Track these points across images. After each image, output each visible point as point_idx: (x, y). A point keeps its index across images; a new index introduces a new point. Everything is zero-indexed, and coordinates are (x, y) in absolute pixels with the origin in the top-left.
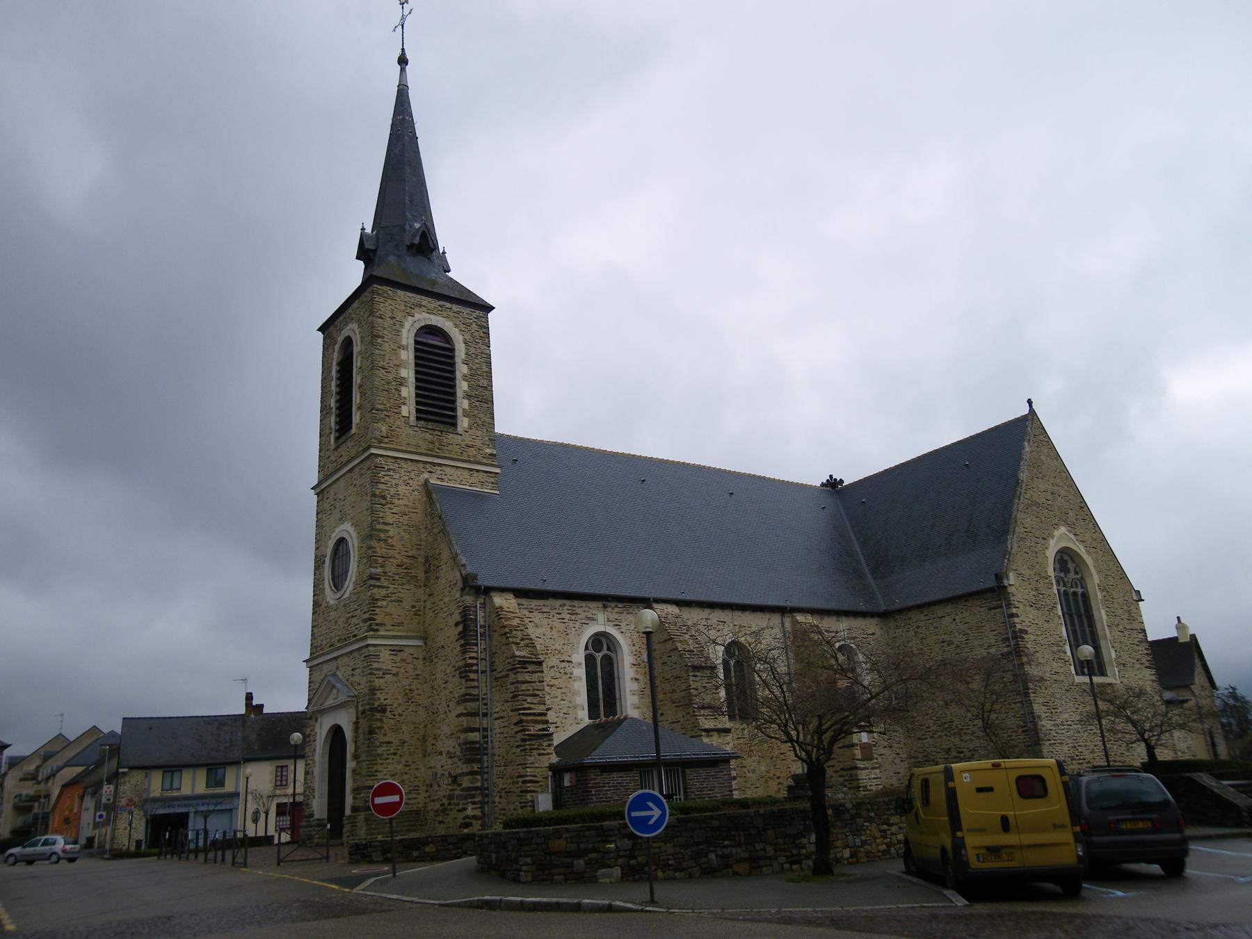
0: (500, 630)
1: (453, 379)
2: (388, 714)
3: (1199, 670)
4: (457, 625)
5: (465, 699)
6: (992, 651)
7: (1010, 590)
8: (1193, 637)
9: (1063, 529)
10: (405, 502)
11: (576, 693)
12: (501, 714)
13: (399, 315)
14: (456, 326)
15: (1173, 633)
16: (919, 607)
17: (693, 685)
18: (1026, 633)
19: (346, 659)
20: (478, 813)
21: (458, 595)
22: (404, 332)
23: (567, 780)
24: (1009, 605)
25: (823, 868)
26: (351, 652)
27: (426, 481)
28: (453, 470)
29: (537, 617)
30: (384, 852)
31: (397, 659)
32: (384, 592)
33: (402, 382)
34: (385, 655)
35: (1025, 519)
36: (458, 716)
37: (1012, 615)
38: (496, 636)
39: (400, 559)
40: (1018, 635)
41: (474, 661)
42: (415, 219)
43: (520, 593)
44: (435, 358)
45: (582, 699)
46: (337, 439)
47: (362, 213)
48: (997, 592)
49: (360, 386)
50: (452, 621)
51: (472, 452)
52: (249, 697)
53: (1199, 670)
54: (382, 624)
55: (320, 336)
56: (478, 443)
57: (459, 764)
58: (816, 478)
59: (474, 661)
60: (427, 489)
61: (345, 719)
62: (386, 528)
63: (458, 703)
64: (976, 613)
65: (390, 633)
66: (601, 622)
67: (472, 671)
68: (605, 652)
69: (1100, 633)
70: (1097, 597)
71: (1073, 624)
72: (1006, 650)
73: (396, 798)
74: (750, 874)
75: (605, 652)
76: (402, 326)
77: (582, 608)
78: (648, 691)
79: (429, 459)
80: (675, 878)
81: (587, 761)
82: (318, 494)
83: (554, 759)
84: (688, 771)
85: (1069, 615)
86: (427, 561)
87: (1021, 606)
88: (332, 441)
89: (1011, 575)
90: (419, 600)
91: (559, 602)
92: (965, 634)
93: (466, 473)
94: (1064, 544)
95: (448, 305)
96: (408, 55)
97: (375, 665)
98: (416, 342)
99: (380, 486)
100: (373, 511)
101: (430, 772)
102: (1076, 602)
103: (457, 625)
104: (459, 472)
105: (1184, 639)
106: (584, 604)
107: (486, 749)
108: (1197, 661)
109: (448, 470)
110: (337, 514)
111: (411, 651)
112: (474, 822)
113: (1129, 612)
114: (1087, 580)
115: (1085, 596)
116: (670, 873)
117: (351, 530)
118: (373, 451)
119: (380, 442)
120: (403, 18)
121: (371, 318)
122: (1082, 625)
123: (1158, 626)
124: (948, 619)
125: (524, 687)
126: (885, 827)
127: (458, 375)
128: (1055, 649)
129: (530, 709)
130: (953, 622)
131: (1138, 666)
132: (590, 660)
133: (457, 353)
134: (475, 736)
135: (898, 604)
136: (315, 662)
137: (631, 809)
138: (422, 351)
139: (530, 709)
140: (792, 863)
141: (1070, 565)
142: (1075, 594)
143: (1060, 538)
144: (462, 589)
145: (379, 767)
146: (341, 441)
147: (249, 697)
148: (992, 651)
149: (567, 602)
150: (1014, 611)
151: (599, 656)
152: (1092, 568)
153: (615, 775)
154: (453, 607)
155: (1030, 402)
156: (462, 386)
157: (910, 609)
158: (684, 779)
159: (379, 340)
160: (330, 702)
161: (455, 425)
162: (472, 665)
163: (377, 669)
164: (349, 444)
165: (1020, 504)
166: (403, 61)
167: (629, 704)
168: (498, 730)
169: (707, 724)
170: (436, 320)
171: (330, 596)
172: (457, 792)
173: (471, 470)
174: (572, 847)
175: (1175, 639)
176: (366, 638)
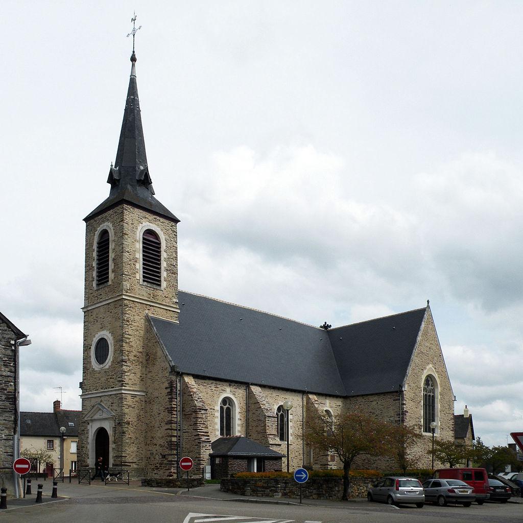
1: (160, 260)
3: (469, 430)
6: (392, 419)
8: (471, 415)
9: (431, 366)
11: (216, 424)
12: (188, 431)
16: (362, 396)
18: (407, 412)
20: (175, 471)
23: (217, 461)
27: (147, 315)
28: (159, 309)
29: (201, 387)
33: (136, 260)
34: (129, 397)
35: (415, 359)
37: (404, 404)
38: (186, 395)
39: (135, 353)
40: (404, 413)
41: (175, 406)
43: (196, 377)
45: (218, 426)
47: (108, 156)
51: (168, 300)
53: (469, 430)
56: (170, 296)
58: (318, 324)
59: (175, 406)
60: (148, 319)
61: (108, 426)
62: (129, 337)
64: (388, 401)
65: (131, 389)
66: (228, 392)
67: (174, 411)
68: (227, 406)
70: (438, 397)
71: (426, 410)
72: (398, 419)
73: (190, 464)
74: (317, 499)
75: (227, 406)
76: (137, 229)
77: (221, 386)
80: (296, 498)
81: (229, 454)
82: (85, 312)
83: (211, 452)
87: (408, 400)
88: (94, 285)
89: (406, 386)
92: (379, 410)
95: (158, 218)
96: (136, 56)
99: (127, 316)
102: (429, 399)
103: (166, 388)
104: (162, 310)
105: (466, 416)
106: (221, 383)
107: (179, 445)
109: (156, 309)
110: (98, 325)
111: (140, 397)
112: (174, 475)
114: (436, 390)
115: (433, 397)
119: (127, 292)
120: (134, 30)
121: (121, 223)
122: (429, 410)
123: (459, 409)
125: (200, 420)
126: (359, 487)
128: (417, 420)
129: (202, 430)
132: (221, 408)
137: (295, 475)
138: (145, 242)
139: (202, 430)
140: (329, 496)
141: (430, 383)
142: (430, 395)
143: (429, 370)
144: (171, 372)
145: (127, 448)
148: (392, 419)
149: (214, 382)
151: (225, 407)
152: (439, 384)
153: (238, 461)
155: (428, 302)
156: (164, 264)
157: (358, 396)
161: (160, 285)
163: (126, 405)
166: (133, 59)
167: (236, 430)
168: (185, 437)
170: (153, 227)
172: (165, 462)
173: (167, 310)
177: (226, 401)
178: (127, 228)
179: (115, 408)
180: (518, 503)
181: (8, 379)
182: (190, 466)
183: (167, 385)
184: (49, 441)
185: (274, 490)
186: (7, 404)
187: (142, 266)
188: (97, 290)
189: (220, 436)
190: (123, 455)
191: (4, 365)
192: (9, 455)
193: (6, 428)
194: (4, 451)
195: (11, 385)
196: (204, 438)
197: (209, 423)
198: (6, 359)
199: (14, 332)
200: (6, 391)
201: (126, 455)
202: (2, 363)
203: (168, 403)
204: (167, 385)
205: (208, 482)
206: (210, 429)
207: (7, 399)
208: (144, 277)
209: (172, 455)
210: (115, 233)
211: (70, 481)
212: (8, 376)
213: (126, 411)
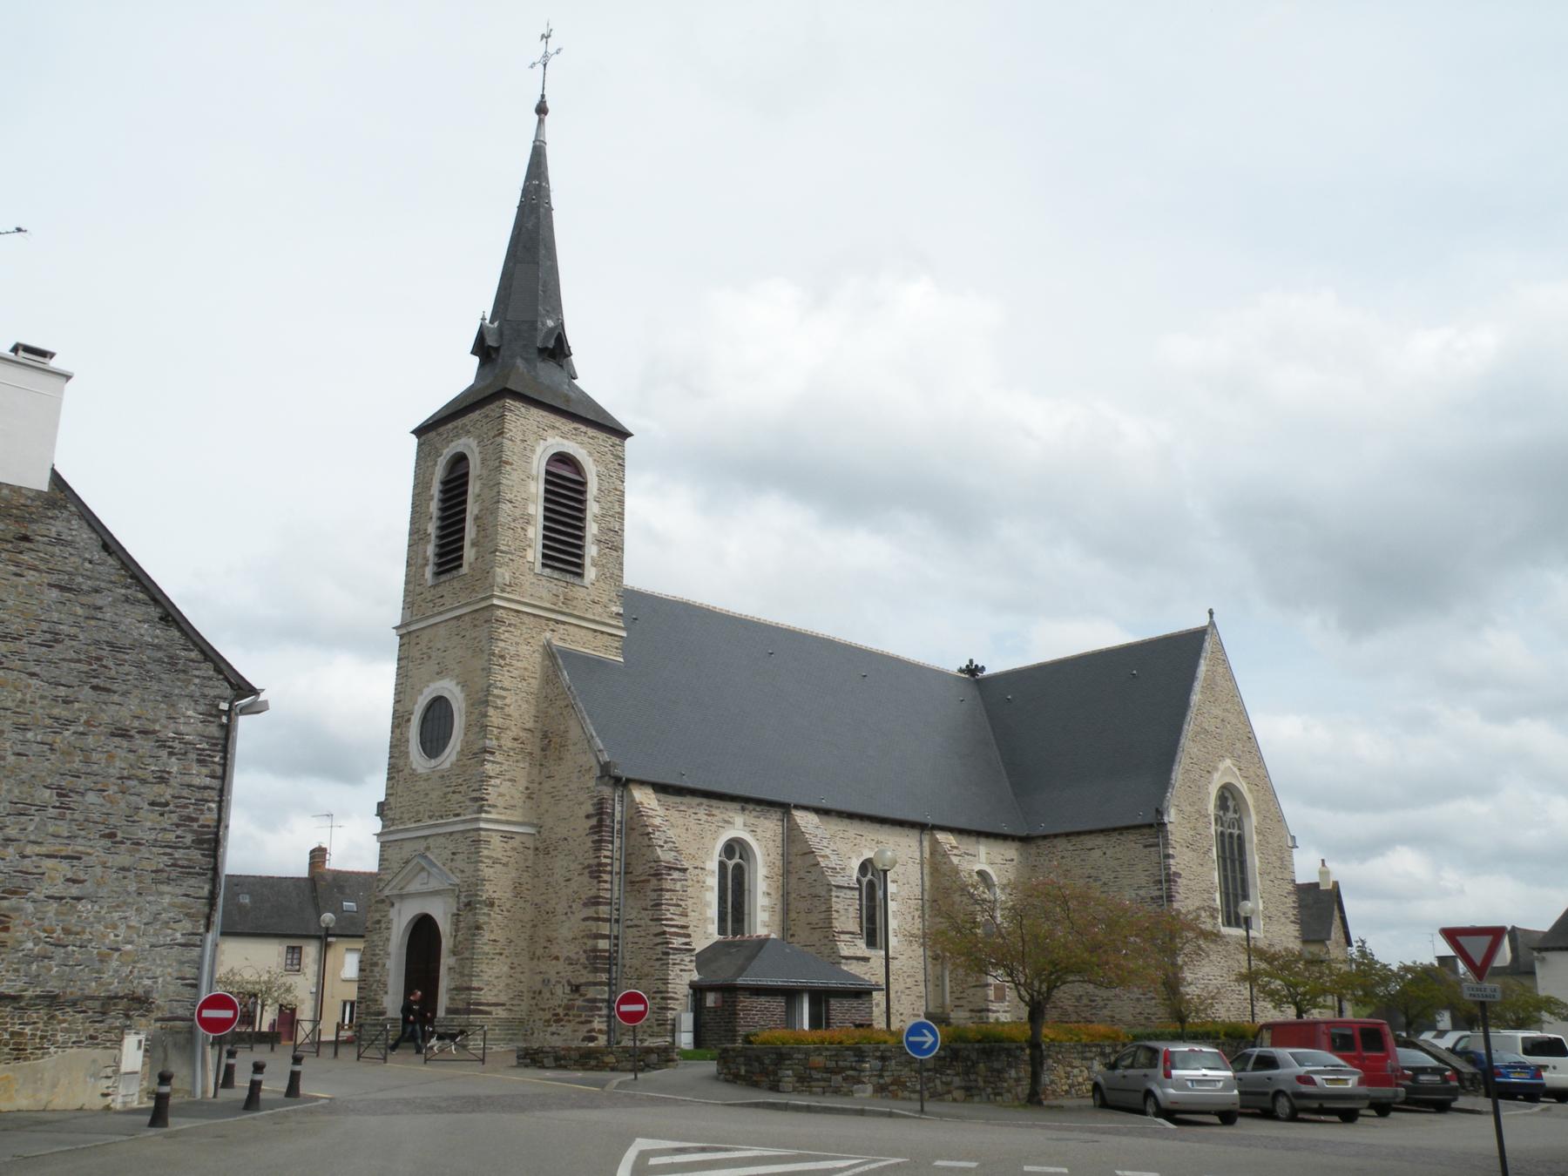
0: (636, 825)
2: (496, 909)
3: (1337, 922)
4: (588, 817)
6: (1142, 893)
7: (1169, 827)
8: (1336, 884)
9: (1228, 762)
11: (708, 905)
12: (635, 922)
14: (590, 454)
15: (1315, 879)
16: (1067, 835)
18: (1179, 875)
19: (442, 840)
21: (592, 783)
22: (535, 458)
23: (710, 1000)
24: (1166, 844)
25: (1034, 1099)
26: (451, 834)
30: (557, 1059)
32: (497, 768)
34: (496, 840)
35: (1190, 747)
36: (585, 919)
39: (515, 732)
42: (548, 314)
43: (661, 789)
44: (565, 488)
46: (437, 574)
48: (1157, 827)
49: (477, 518)
50: (582, 813)
51: (599, 609)
53: (1337, 922)
54: (494, 806)
55: (414, 440)
56: (605, 599)
57: (584, 972)
58: (953, 663)
60: (550, 653)
62: (503, 693)
63: (585, 905)
64: (1131, 847)
65: (503, 818)
66: (738, 825)
68: (737, 860)
69: (1250, 881)
71: (1225, 870)
72: (1157, 893)
73: (640, 1008)
74: (964, 1101)
75: (737, 860)
76: (533, 451)
77: (723, 811)
79: (554, 616)
81: (740, 981)
82: (401, 637)
83: (695, 976)
84: (832, 1001)
85: (1222, 858)
89: (1173, 811)
90: (532, 782)
91: (698, 800)
93: (590, 634)
94: (1227, 779)
95: (583, 428)
97: (486, 852)
98: (548, 472)
99: (501, 644)
101: (539, 978)
102: (1231, 844)
103: (588, 817)
108: (1336, 913)
109: (571, 629)
113: (1281, 859)
114: (1245, 821)
115: (1240, 838)
116: (906, 1094)
117: (457, 690)
120: (546, 56)
122: (1234, 871)
123: (1305, 868)
124: (1097, 853)
127: (589, 516)
128: (1206, 896)
130: (1102, 856)
131: (1283, 920)
134: (603, 944)
135: (1043, 828)
136: (392, 838)
138: (551, 479)
141: (1231, 803)
142: (1231, 835)
143: (1225, 772)
146: (443, 578)
148: (1142, 893)
149: (705, 801)
150: (1171, 851)
151: (731, 864)
154: (583, 797)
155: (1211, 613)
156: (592, 529)
158: (828, 1010)
159: (508, 468)
160: (414, 887)
161: (581, 575)
162: (606, 865)
164: (455, 583)
165: (1189, 729)
166: (542, 110)
169: (845, 951)
171: (417, 759)
172: (579, 1003)
174: (833, 1064)
175: (1317, 885)
176: (478, 820)
177: (731, 848)
178: (511, 449)
182: (640, 1015)
183: (591, 810)
186: (196, 855)
187: (541, 532)
188: (434, 586)
189: (716, 937)
190: (475, 984)
191: (199, 761)
194: (175, 974)
195: (210, 809)
197: (690, 902)
199: (230, 683)
200: (195, 825)
204: (591, 810)
205: (686, 1055)
207: (198, 842)
208: (545, 556)
209: (595, 984)
210: (483, 461)
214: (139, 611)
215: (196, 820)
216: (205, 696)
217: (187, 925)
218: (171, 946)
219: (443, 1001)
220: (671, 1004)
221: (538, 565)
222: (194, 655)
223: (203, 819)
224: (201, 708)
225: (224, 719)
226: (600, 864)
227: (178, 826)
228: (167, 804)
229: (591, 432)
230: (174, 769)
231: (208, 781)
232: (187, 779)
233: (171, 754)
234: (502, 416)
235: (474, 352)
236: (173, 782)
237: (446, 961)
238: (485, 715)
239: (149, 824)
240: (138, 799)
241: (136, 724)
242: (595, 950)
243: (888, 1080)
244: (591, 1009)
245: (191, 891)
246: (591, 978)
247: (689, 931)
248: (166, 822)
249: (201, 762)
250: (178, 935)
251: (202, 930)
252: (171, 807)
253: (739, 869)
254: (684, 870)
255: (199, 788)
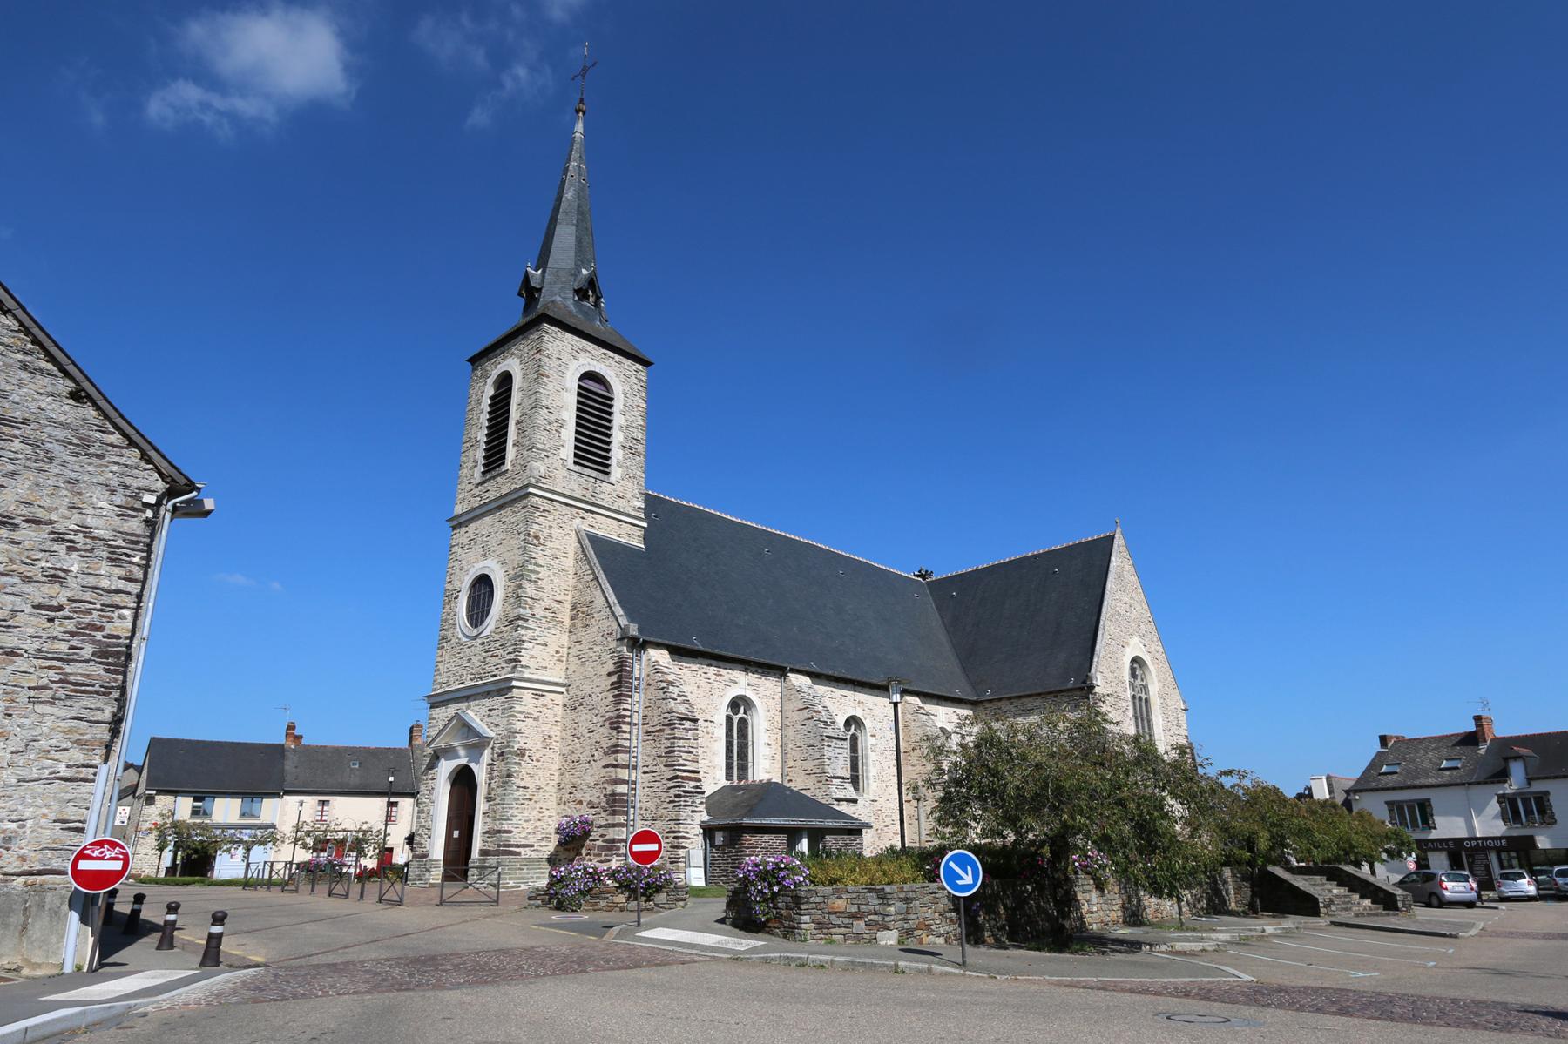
4: (609, 674)
5: (615, 749)
10: (556, 545)
13: (565, 358)
17: (827, 755)
22: (569, 374)
23: (719, 838)
31: (538, 703)
32: (530, 633)
46: (484, 473)
48: (1087, 688)
52: (291, 727)
56: (628, 496)
63: (606, 753)
73: (654, 847)
78: (779, 757)
83: (705, 817)
84: (828, 838)
86: (574, 607)
97: (518, 708)
98: (580, 387)
100: (524, 551)
103: (609, 674)
115: (1147, 700)
118: (531, 490)
125: (680, 743)
132: (729, 720)
133: (615, 403)
134: (622, 789)
138: (582, 392)
145: (516, 812)
147: (291, 727)
151: (736, 719)
153: (766, 837)
154: (606, 657)
174: (854, 909)
177: (736, 703)
178: (549, 365)
179: (497, 720)
180: (1444, 935)
181: (118, 599)
182: (652, 856)
183: (612, 668)
184: (392, 804)
185: (876, 923)
186: (97, 670)
187: (573, 435)
188: (481, 483)
189: (724, 782)
190: (505, 827)
191: (111, 560)
192: (69, 829)
193: (77, 742)
194: (53, 816)
195: (121, 617)
196: (690, 785)
197: (700, 751)
198: (120, 542)
199: (160, 474)
200: (99, 636)
201: (510, 828)
202: (105, 554)
203: (612, 707)
204: (612, 668)
205: (697, 892)
206: (702, 766)
207: (102, 654)
208: (576, 455)
209: (614, 826)
210: (525, 375)
211: (362, 895)
212: (118, 592)
213: (518, 725)
214: (42, 382)
215: (101, 629)
216: (125, 486)
217: (78, 756)
218: (49, 780)
219: (477, 844)
220: (684, 843)
221: (571, 459)
222: (115, 438)
223: (110, 629)
224: (119, 499)
225: (149, 514)
226: (619, 716)
227: (73, 634)
228: (60, 608)
229: (618, 358)
230: (75, 568)
231: (121, 585)
232: (91, 581)
233: (70, 549)
234: (541, 337)
235: (520, 294)
236: (70, 582)
237: (481, 806)
238: (520, 587)
239: (31, 631)
240: (18, 599)
241: (24, 510)
242: (614, 794)
243: (912, 924)
244: (610, 849)
245: (86, 714)
246: (611, 820)
247: (701, 775)
248: (56, 629)
249: (113, 561)
250: (62, 768)
251: (97, 760)
252: (66, 612)
253: (743, 722)
254: (695, 721)
255: (109, 592)
